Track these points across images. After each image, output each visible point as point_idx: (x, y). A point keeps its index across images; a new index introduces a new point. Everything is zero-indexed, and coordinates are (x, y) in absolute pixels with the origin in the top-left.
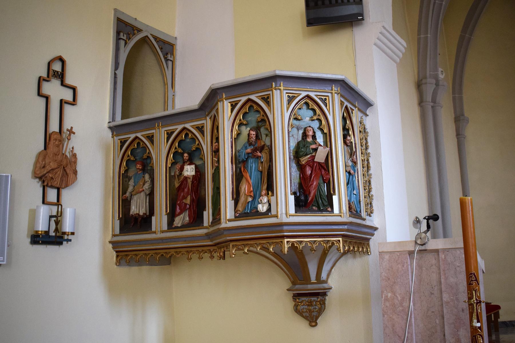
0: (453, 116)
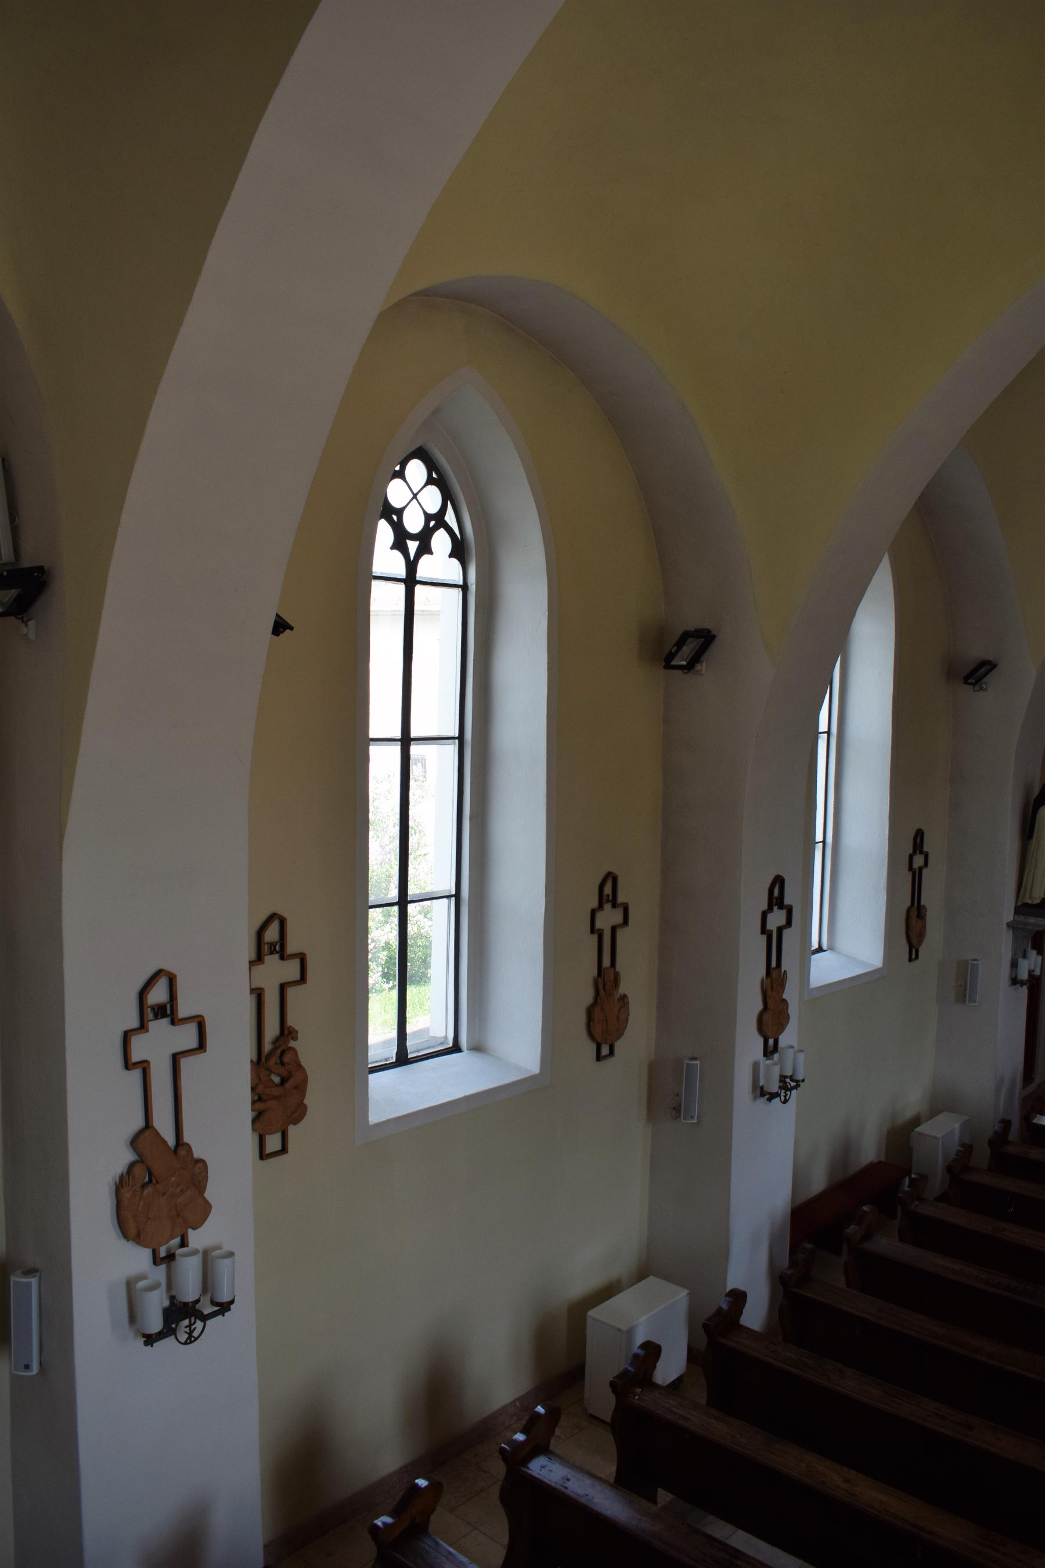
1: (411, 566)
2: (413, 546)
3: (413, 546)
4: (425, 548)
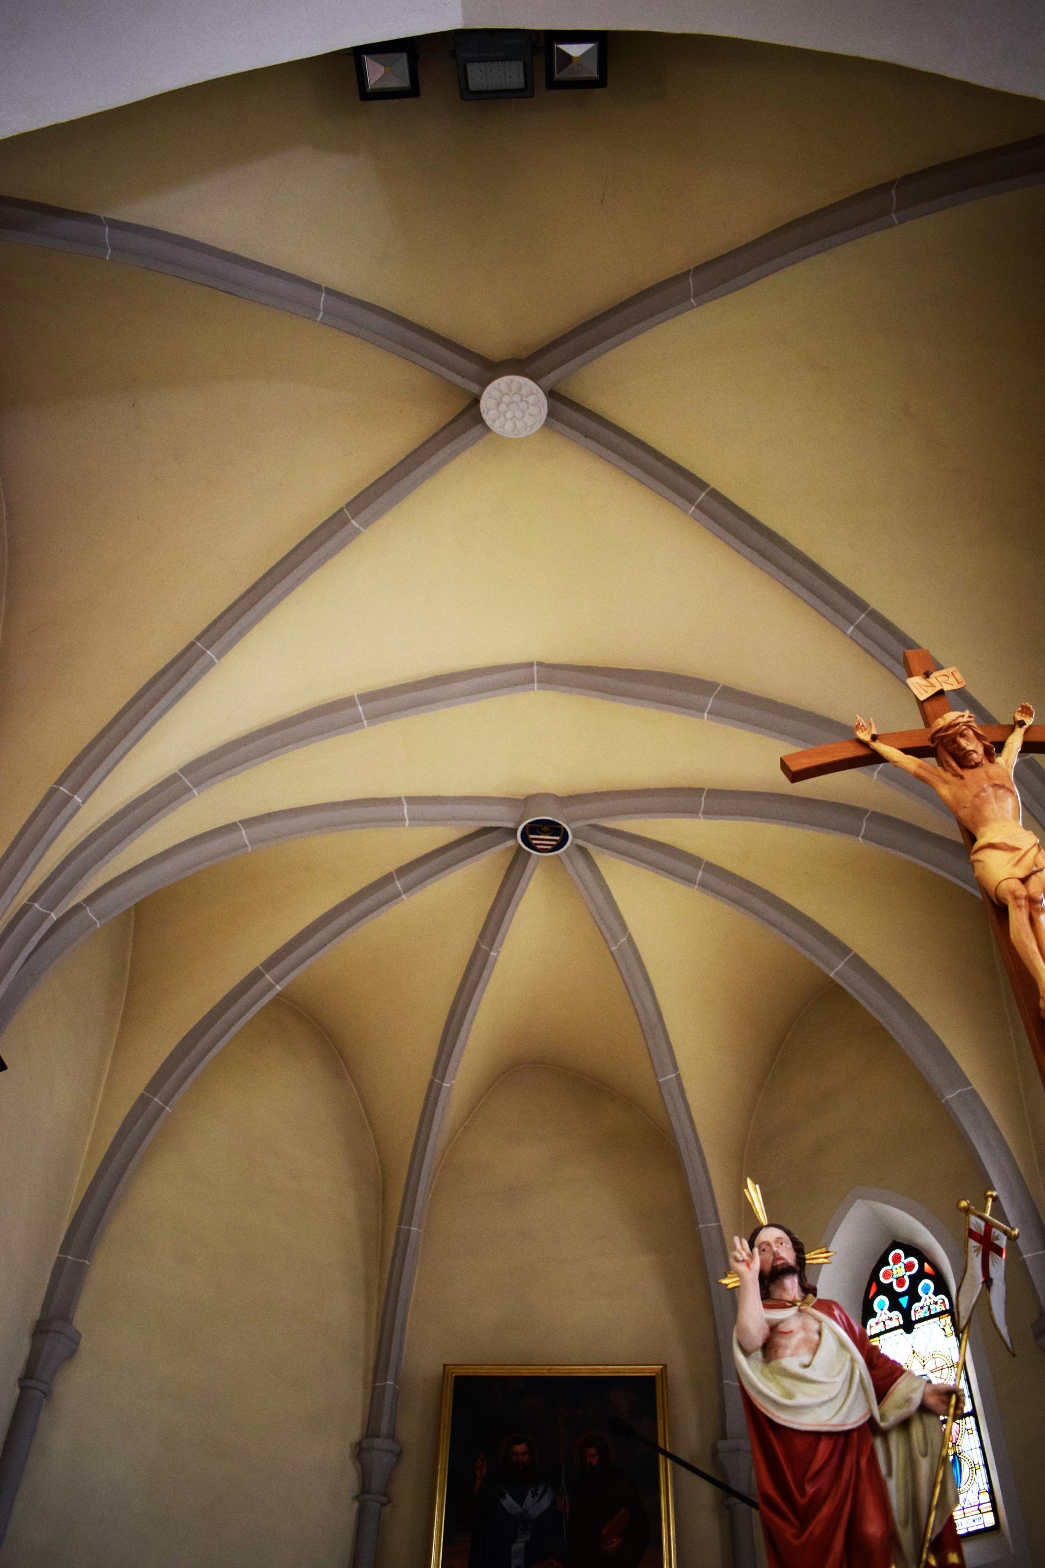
0: (35, 1312)
1: (906, 1313)
2: (904, 1301)
3: (904, 1301)
4: (914, 1297)
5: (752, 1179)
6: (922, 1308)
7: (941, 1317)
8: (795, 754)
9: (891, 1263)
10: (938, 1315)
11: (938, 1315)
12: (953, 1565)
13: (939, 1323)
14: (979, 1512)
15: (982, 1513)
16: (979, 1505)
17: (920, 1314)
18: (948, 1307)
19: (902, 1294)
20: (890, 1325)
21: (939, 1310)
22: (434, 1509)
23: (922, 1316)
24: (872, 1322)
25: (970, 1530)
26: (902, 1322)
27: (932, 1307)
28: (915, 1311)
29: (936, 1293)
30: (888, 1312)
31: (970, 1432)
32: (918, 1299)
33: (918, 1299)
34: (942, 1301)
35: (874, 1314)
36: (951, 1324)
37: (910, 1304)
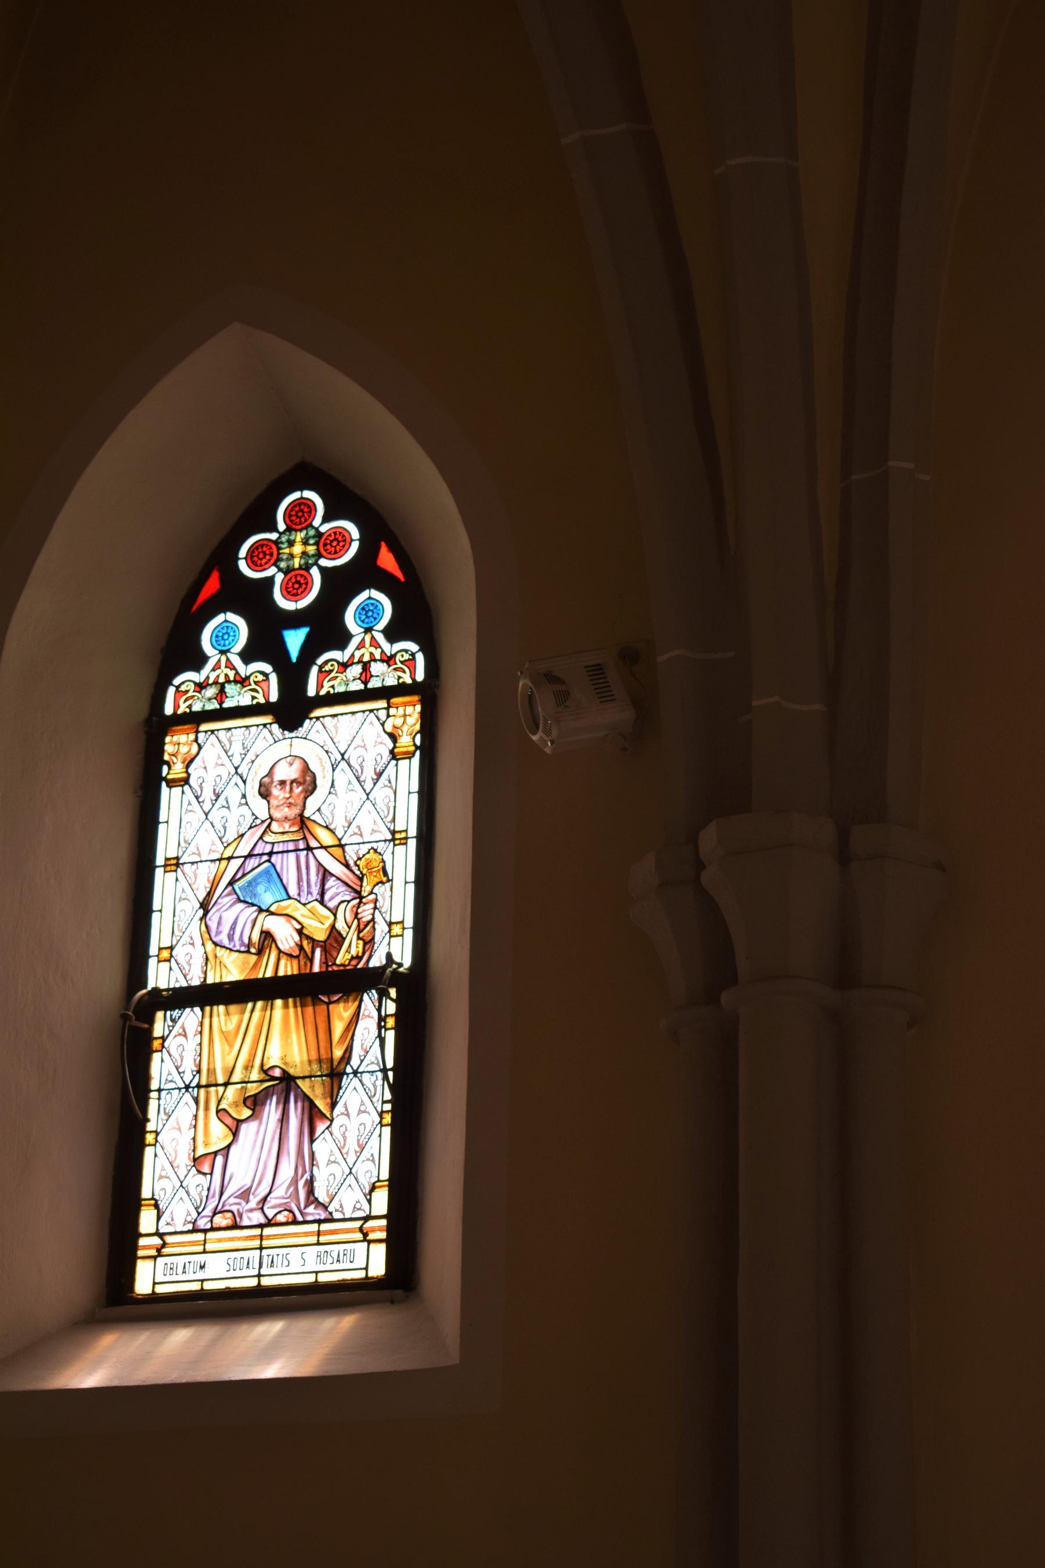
2: (294, 640)
5: (321, 995)
6: (344, 666)
7: (394, 700)
8: (387, 1083)
9: (282, 526)
10: (386, 693)
11: (386, 693)
12: (392, 1118)
13: (382, 714)
14: (360, 1236)
15: (370, 1242)
16: (367, 1218)
17: (335, 683)
18: (420, 676)
19: (295, 620)
20: (238, 697)
21: (391, 681)
22: (133, 1091)
23: (341, 689)
24: (187, 678)
25: (323, 1278)
26: (274, 697)
27: (377, 668)
28: (320, 671)
29: (393, 634)
30: (237, 661)
31: (397, 929)
32: (342, 639)
33: (342, 639)
34: (407, 657)
35: (198, 661)
36: (418, 727)
37: (310, 651)
